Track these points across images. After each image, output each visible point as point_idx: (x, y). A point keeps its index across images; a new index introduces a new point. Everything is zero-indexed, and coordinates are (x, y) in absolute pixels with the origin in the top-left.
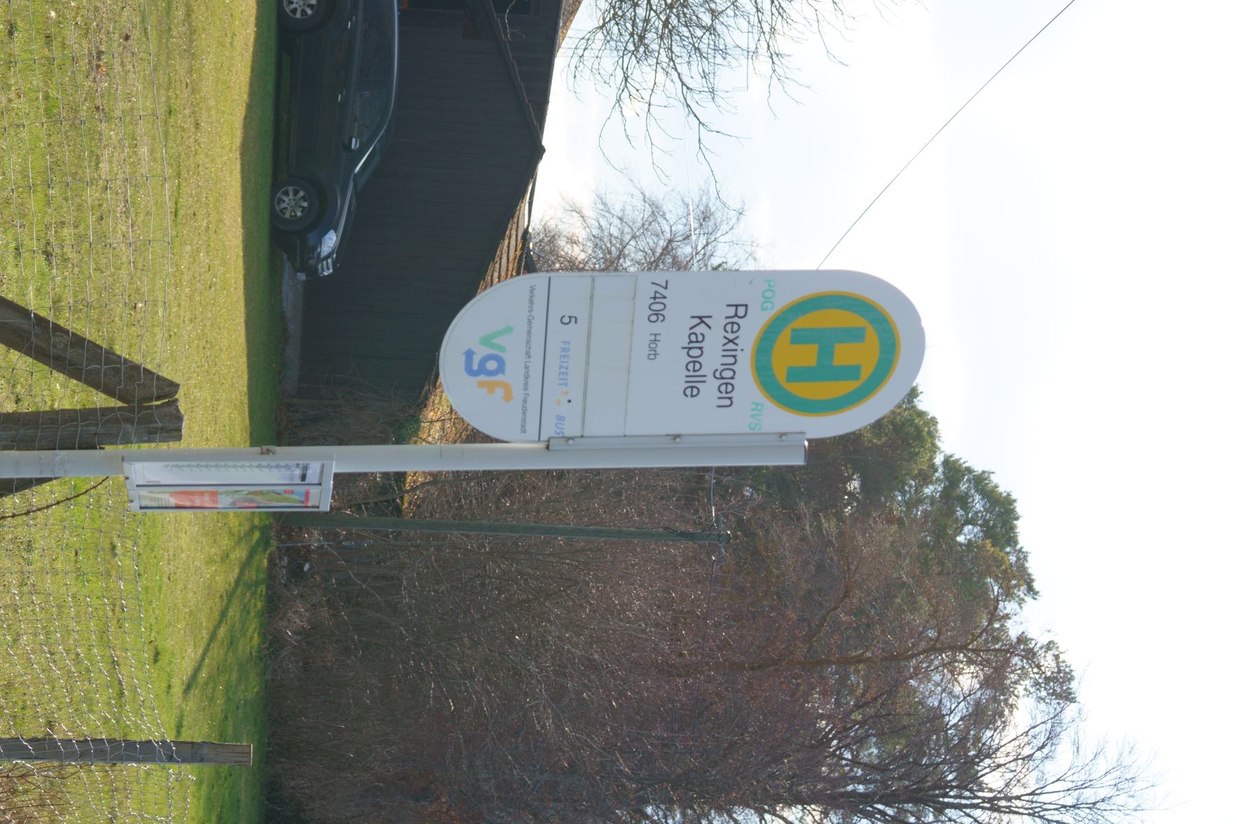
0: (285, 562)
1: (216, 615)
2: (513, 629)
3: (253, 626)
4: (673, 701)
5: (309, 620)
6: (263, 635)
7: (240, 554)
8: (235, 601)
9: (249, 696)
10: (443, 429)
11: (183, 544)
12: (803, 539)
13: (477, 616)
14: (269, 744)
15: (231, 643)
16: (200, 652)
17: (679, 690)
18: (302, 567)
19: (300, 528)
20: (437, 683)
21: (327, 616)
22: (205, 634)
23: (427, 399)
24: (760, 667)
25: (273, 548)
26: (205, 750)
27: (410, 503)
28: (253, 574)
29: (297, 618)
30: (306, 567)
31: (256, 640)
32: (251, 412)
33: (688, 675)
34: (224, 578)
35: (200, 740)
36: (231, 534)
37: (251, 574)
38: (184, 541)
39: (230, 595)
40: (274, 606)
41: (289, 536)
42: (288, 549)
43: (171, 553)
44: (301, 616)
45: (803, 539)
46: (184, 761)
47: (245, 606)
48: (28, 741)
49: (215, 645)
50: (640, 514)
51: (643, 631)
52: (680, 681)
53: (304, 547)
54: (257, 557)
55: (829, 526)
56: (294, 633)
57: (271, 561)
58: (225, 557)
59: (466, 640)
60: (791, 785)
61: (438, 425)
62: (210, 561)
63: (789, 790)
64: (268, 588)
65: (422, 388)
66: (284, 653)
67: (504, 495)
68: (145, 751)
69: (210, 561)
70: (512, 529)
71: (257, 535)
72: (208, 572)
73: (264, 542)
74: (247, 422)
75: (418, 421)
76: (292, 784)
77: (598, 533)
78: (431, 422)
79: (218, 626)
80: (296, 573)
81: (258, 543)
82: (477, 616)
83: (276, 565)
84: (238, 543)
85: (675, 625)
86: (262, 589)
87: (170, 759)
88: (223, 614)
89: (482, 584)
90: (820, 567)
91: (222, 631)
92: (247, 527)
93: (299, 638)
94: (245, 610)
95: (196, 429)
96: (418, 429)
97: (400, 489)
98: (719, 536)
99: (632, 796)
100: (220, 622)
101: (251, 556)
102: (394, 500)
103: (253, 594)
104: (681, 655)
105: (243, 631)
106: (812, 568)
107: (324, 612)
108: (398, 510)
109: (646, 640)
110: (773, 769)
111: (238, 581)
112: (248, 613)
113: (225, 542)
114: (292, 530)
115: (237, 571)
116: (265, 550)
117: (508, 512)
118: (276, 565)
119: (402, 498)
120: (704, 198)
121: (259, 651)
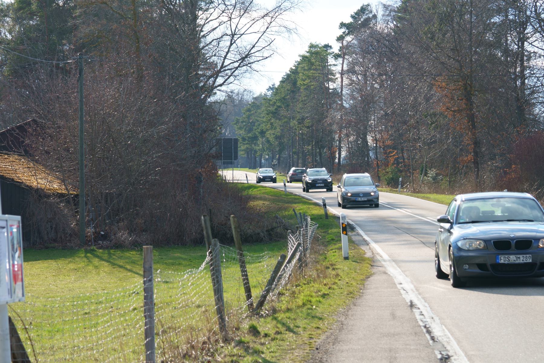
0: (100, 242)
1: (121, 270)
2: (125, 144)
3: (127, 254)
4: (153, 75)
5: (125, 231)
6: (132, 249)
7: (96, 261)
8: (116, 262)
9: (157, 254)
10: (41, 179)
11: (90, 285)
12: (84, 23)
13: (120, 160)
14: (178, 244)
15: (134, 263)
16: (136, 275)
17: (148, 73)
18: (102, 235)
19: (86, 236)
20: (150, 175)
21: (122, 223)
22: (129, 274)
23: (28, 186)
24: (138, 39)
25: (95, 248)
26: (147, 266)
27: (74, 191)
28: (106, 255)
29: (124, 236)
30: (102, 233)
31: (134, 253)
32: (36, 260)
33: (142, 69)
34: (105, 267)
35: (143, 269)
36: (88, 265)
37: (106, 256)
38: (89, 285)
39: (113, 264)
40: (119, 246)
41: (90, 241)
42: (95, 241)
43: (93, 290)
44: (123, 234)
45: (84, 23)
46: (152, 275)
47: (119, 258)
48: (146, 339)
49: (134, 270)
50: (74, 93)
51: (124, 89)
52: (145, 73)
53: (94, 235)
54: (98, 254)
55: (78, 12)
56: (130, 236)
57: (100, 248)
58: (96, 267)
59: (130, 164)
60: (187, 24)
61: (39, 180)
62: (98, 274)
63: (189, 24)
64: (112, 249)
65: (23, 188)
66: (139, 240)
67: (68, 151)
68: (148, 292)
69: (98, 274)
70: (82, 147)
71: (89, 255)
72: (102, 274)
73: (92, 251)
74: (40, 261)
75: (38, 189)
76: (194, 234)
77: (81, 110)
78: (38, 183)
79: (127, 269)
80: (105, 237)
81: (92, 254)
82: (120, 160)
83: (102, 246)
84: (90, 261)
85: (120, 75)
86: (112, 251)
87: (150, 280)
88: (121, 267)
89: (107, 158)
90: (95, 15)
91: (128, 267)
92: (85, 259)
93: (132, 234)
94: (120, 258)
95: (41, 282)
96: (41, 189)
97: (67, 195)
98: (80, 58)
99: (195, 91)
100: (124, 268)
101: (98, 257)
102: (72, 198)
103: (114, 255)
104: (133, 73)
105: (129, 258)
106: (96, 19)
107: (121, 224)
108: (76, 196)
109: (127, 88)
110: (181, 32)
111: (108, 261)
112: (122, 257)
113: (91, 267)
114: (87, 240)
115: (104, 262)
116: (96, 251)
117: (75, 148)
118: (102, 246)
119: (72, 194)
120: (529, 35)
121: (138, 251)
